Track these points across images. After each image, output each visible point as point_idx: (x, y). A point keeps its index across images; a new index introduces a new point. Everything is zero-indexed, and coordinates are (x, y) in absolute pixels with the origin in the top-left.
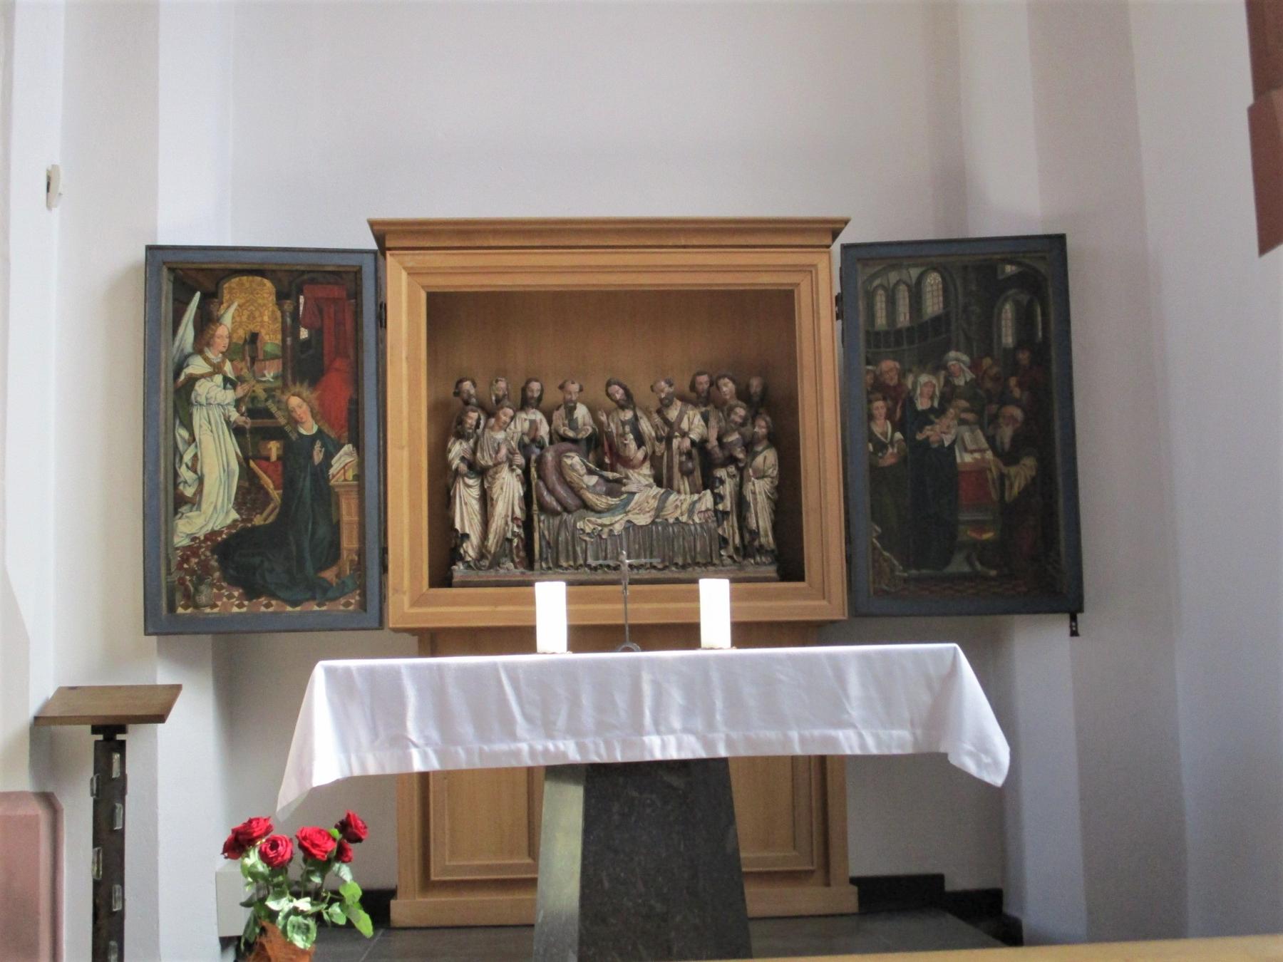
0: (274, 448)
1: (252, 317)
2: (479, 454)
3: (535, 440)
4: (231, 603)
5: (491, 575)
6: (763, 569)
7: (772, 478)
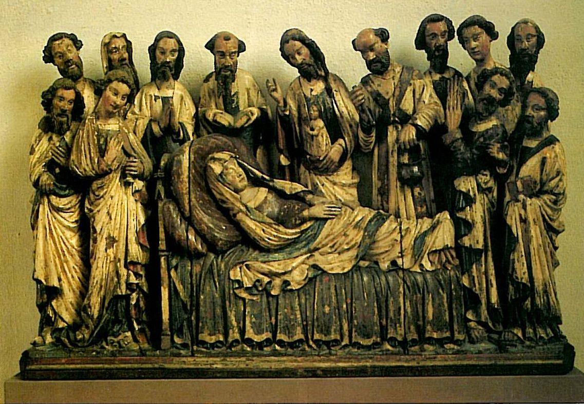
2: (73, 157)
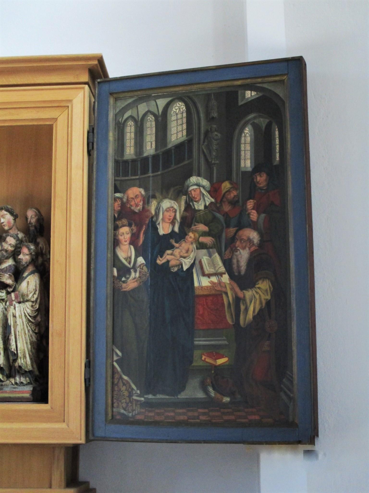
6: (21, 388)
7: (33, 302)
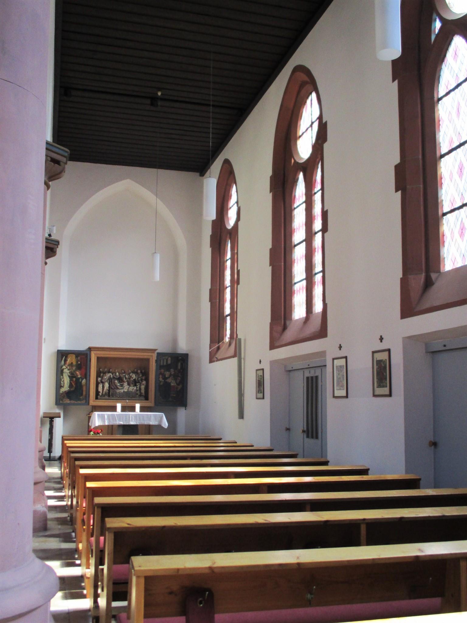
0: (74, 379)
1: (72, 360)
3: (111, 378)
4: (68, 401)
5: (103, 398)
